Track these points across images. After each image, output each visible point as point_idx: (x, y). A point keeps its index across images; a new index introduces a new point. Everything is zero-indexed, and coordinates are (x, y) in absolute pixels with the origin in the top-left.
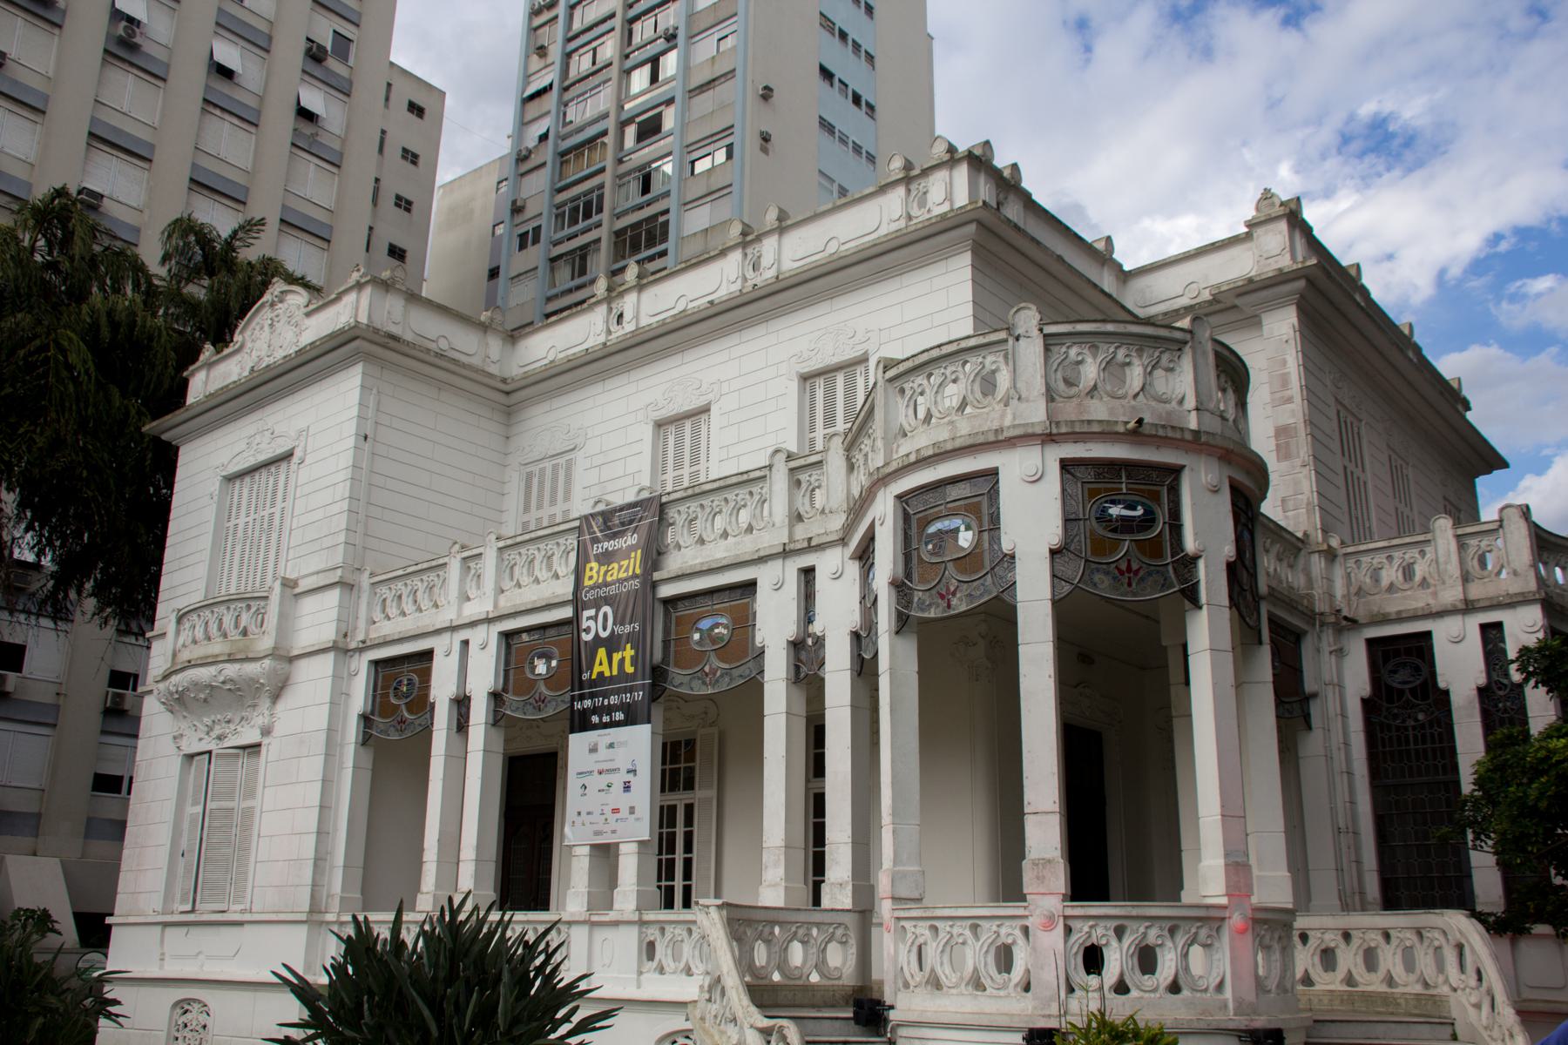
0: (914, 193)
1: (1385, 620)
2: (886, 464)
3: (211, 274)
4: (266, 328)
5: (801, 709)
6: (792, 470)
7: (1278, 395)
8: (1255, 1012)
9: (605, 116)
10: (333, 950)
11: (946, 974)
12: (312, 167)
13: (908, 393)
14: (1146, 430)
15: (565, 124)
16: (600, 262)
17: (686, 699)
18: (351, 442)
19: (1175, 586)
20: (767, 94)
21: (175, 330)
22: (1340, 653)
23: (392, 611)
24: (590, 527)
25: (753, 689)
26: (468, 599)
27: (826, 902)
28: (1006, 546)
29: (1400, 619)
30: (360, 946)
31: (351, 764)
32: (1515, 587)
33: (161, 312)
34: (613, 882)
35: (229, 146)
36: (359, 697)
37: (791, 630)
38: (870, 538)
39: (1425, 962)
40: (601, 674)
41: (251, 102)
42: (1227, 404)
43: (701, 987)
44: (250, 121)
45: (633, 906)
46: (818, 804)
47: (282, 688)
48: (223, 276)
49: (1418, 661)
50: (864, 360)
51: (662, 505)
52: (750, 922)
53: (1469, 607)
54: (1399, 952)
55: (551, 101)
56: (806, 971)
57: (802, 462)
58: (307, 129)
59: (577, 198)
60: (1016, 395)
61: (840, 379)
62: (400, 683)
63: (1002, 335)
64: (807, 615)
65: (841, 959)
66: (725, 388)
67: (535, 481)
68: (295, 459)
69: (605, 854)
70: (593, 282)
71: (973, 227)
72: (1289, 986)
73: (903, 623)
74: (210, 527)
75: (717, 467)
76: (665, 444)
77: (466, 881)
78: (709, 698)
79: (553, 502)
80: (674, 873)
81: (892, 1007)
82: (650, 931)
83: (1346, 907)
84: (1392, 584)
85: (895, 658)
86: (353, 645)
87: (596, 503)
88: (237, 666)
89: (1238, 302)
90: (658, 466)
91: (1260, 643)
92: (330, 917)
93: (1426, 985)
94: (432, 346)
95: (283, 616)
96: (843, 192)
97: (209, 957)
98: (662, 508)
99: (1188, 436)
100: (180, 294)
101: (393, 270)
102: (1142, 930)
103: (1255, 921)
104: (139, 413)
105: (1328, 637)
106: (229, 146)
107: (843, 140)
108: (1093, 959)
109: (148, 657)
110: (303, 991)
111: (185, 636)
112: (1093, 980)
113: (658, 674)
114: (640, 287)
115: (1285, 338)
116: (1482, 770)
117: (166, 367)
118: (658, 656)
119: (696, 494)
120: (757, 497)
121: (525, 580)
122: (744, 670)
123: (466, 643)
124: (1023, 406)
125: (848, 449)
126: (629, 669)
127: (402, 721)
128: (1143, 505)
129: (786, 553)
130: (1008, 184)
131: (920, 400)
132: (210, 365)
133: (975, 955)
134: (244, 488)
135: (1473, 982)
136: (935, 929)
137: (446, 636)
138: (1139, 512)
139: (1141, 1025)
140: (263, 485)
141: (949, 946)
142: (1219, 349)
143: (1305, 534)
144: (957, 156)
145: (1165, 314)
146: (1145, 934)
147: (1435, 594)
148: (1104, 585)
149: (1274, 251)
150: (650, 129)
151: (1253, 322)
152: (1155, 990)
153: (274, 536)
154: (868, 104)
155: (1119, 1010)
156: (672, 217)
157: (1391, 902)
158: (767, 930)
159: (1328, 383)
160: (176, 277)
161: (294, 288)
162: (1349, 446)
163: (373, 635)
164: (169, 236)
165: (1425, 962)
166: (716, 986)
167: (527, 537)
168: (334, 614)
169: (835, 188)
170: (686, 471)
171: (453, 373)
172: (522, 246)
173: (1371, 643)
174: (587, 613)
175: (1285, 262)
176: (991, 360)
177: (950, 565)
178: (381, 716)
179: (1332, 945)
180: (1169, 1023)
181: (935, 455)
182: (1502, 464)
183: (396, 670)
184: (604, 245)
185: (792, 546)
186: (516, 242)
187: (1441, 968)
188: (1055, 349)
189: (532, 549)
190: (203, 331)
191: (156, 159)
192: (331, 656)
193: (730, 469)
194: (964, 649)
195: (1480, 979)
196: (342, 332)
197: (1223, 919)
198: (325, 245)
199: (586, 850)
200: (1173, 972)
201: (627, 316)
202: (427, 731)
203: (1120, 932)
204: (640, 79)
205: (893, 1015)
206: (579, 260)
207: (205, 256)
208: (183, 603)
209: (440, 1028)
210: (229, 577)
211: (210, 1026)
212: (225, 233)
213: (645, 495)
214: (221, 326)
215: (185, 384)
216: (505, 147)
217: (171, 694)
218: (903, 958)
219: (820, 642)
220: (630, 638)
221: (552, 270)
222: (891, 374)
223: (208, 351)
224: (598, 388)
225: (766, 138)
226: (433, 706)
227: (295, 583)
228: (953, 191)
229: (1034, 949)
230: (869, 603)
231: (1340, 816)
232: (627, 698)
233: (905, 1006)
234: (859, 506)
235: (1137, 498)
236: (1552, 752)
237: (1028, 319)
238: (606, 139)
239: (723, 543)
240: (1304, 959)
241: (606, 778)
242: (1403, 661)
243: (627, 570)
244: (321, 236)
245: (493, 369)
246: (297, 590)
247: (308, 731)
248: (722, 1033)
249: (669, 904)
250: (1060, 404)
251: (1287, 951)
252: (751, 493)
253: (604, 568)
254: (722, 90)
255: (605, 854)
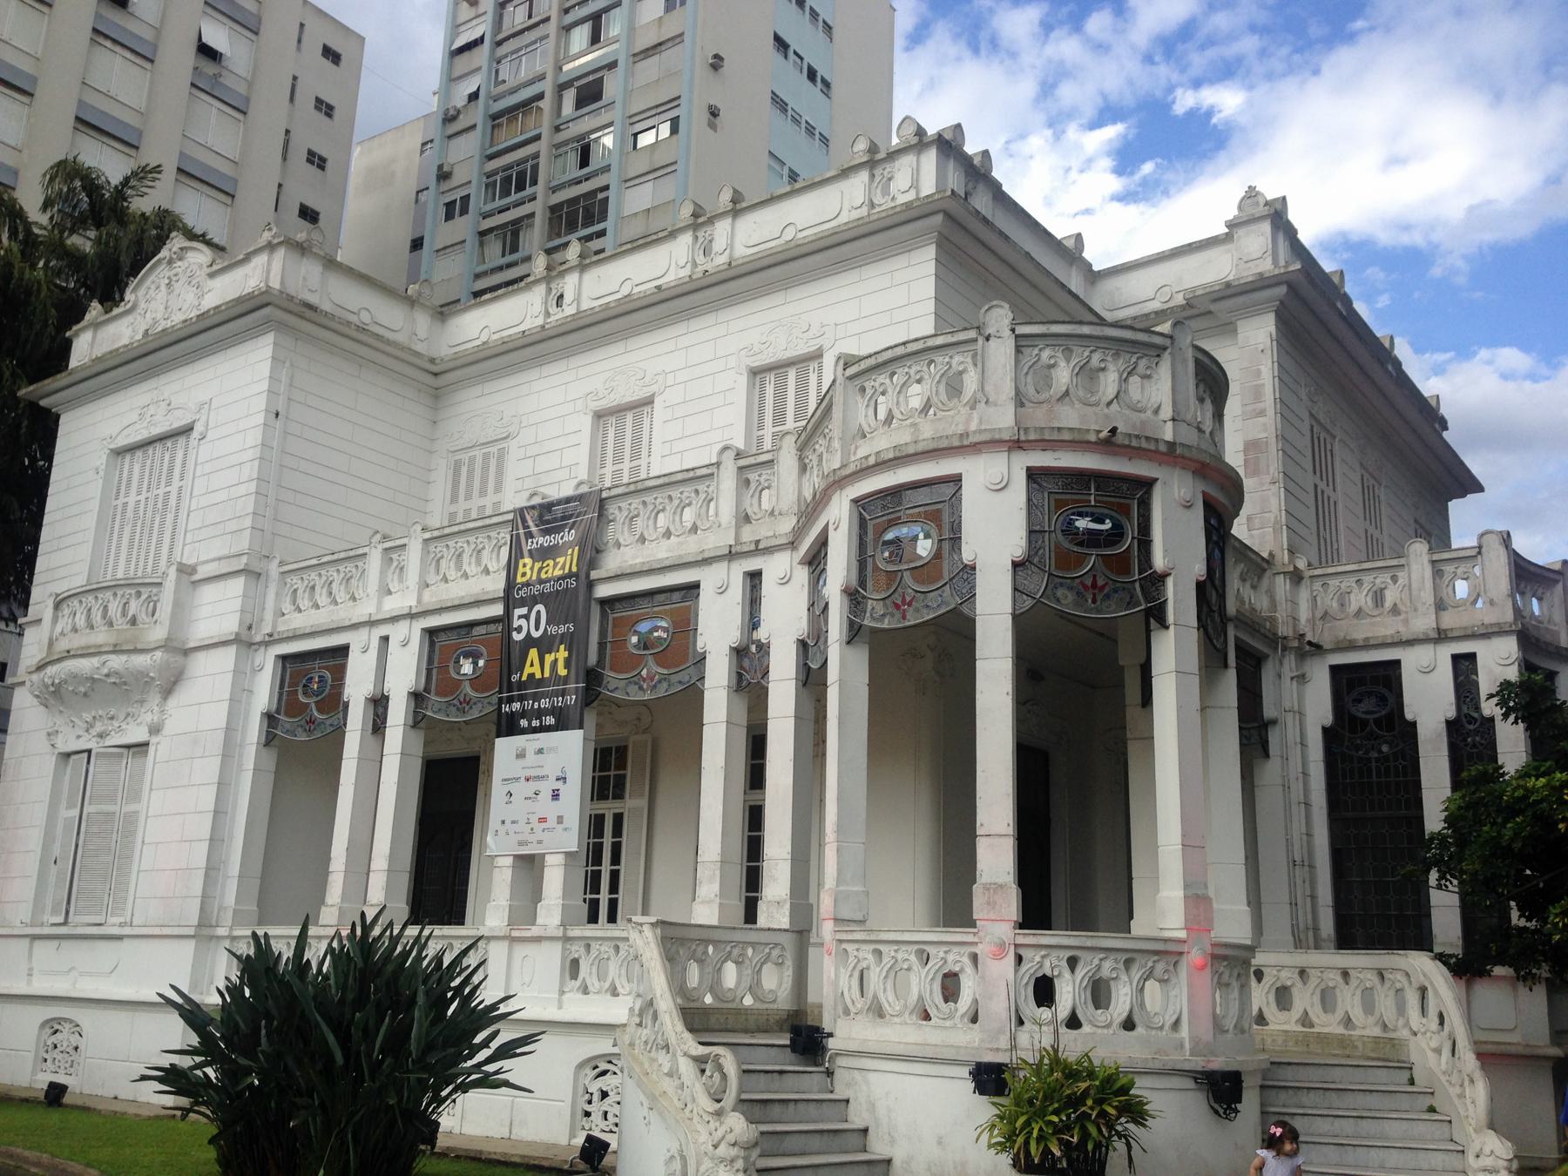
0: (877, 179)
1: (1352, 646)
2: (843, 466)
3: (98, 226)
4: (163, 288)
5: (742, 719)
6: (740, 468)
7: (1250, 408)
8: (1213, 1053)
9: (542, 77)
10: (224, 971)
11: (889, 1001)
12: (214, 111)
13: (869, 392)
14: (1119, 439)
15: (498, 83)
16: (533, 238)
17: (618, 704)
18: (260, 419)
19: (1121, 604)
20: (717, 63)
21: (57, 286)
22: (1301, 679)
23: (304, 603)
24: (524, 521)
25: (693, 696)
26: (390, 593)
27: (762, 921)
28: (967, 556)
29: (1367, 646)
30: (258, 965)
31: (252, 766)
32: (1490, 618)
33: (41, 264)
34: (537, 895)
35: (120, 83)
36: (263, 694)
37: (734, 636)
38: (822, 543)
39: (1385, 1004)
40: (531, 676)
41: (148, 35)
42: (1205, 415)
43: (632, 1010)
44: (145, 56)
45: (557, 920)
46: (755, 817)
47: (175, 683)
48: (113, 228)
49: (1385, 691)
50: (817, 355)
51: (602, 500)
52: (682, 941)
53: (1441, 636)
54: (1359, 993)
55: (482, 55)
56: (739, 994)
57: (751, 461)
58: (209, 68)
59: (509, 167)
60: (982, 398)
61: (792, 374)
62: (311, 681)
63: (972, 334)
64: (753, 621)
65: (776, 983)
66: (670, 380)
67: (464, 470)
68: (195, 434)
69: (529, 865)
70: (528, 259)
71: (939, 218)
72: (1246, 1026)
73: (854, 633)
74: (95, 505)
75: (660, 463)
76: (605, 436)
77: (377, 893)
78: (644, 704)
79: (483, 493)
80: (601, 888)
81: (831, 1035)
82: (574, 948)
83: (1299, 944)
84: (1360, 610)
85: (846, 670)
86: (258, 639)
87: (532, 495)
88: (124, 658)
89: (1212, 307)
90: (597, 458)
91: (1226, 666)
92: (221, 931)
93: (1385, 1027)
94: (353, 318)
95: (178, 605)
96: (793, 176)
97: (81, 974)
98: (602, 503)
99: (1163, 448)
100: (62, 243)
101: (309, 233)
102: (1096, 962)
103: (1214, 957)
104: (13, 374)
105: (1290, 662)
106: (120, 83)
107: (796, 121)
108: (1044, 991)
109: (20, 646)
110: (192, 1014)
111: (64, 623)
112: (1045, 1013)
113: (592, 678)
114: (583, 267)
115: (1261, 347)
116: (1453, 807)
117: (46, 325)
118: (593, 659)
119: (639, 489)
120: (702, 496)
121: (452, 574)
122: (684, 676)
123: (385, 639)
124: (991, 409)
125: (801, 449)
126: (562, 672)
127: (311, 721)
128: (1111, 518)
129: (731, 555)
130: (978, 172)
131: (881, 399)
132: (96, 325)
133: (922, 983)
134: (135, 465)
135: (1434, 1025)
136: (878, 953)
137: (364, 632)
138: (1108, 525)
139: (1096, 1063)
140: (157, 463)
141: (894, 971)
142: (1200, 356)
143: (1271, 554)
144: (926, 140)
145: (1135, 318)
146: (1099, 967)
147: (1406, 621)
148: (1066, 601)
149: (1256, 253)
150: (590, 93)
151: (1228, 329)
152: (1108, 1026)
153: (170, 517)
154: (824, 81)
155: (1073, 1046)
156: (612, 194)
157: (1345, 940)
158: (700, 949)
159: (1304, 398)
160: (58, 227)
161: (195, 244)
162: (1321, 463)
163: (281, 628)
164: (52, 180)
165: (1385, 1004)
166: (648, 1009)
167: (456, 529)
168: (238, 604)
169: (786, 172)
170: (626, 466)
171: (376, 349)
172: (449, 216)
173: (1335, 670)
174: (518, 612)
175: (1266, 266)
176: (958, 360)
177: (907, 575)
178: (287, 714)
179: (1289, 983)
180: (1121, 1062)
181: (895, 459)
182: (1479, 488)
183: (308, 665)
184: (538, 220)
185: (738, 549)
186: (442, 211)
187: (1401, 1009)
188: (1026, 351)
189: (461, 541)
190: (88, 288)
191: (37, 95)
192: (232, 651)
193: (672, 465)
194: (919, 666)
195: (1442, 1023)
196: (250, 297)
197: (1181, 953)
198: (228, 200)
199: (509, 861)
200: (1128, 1008)
201: (568, 298)
202: (339, 732)
203: (1073, 963)
204: (581, 36)
205: (832, 1044)
206: (511, 235)
207: (92, 203)
208: (62, 587)
209: (346, 1056)
210: (117, 555)
211: (82, 1047)
212: (115, 179)
213: (584, 489)
214: (109, 282)
215: (66, 347)
216: (433, 105)
217: (47, 686)
218: (844, 982)
219: (764, 648)
220: (562, 638)
221: (482, 244)
222: (851, 371)
223: (95, 310)
224: (533, 374)
225: (714, 113)
226: (346, 705)
227: (192, 570)
228: (919, 178)
229: (983, 978)
230: (817, 610)
231: (1297, 847)
232: (558, 701)
233: (845, 1034)
234: (811, 509)
235: (1106, 511)
236: (1529, 792)
237: (1000, 318)
238: (541, 104)
239: (665, 543)
240: (1260, 996)
241: (533, 786)
242: (1369, 692)
243: (563, 568)
244: (226, 192)
245: (419, 347)
246: (196, 577)
247: (207, 725)
248: (654, 1060)
249: (593, 918)
250: (1029, 409)
251: (1244, 987)
252: (697, 492)
253: (537, 565)
254: (670, 56)
255: (529, 865)
